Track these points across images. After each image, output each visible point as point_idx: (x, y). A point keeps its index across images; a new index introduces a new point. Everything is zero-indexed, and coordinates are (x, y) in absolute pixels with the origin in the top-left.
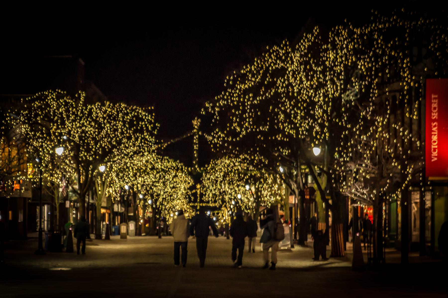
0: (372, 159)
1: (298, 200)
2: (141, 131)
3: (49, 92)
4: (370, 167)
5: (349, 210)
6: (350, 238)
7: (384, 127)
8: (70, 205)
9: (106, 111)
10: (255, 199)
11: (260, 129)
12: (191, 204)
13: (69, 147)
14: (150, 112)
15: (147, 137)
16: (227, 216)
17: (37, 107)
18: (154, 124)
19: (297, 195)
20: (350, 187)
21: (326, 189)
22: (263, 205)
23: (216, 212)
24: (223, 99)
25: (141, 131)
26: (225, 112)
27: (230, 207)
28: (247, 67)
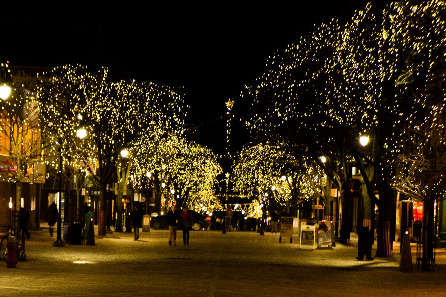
0: (425, 151)
1: (341, 194)
2: (170, 113)
3: (68, 67)
4: (422, 160)
5: (397, 206)
6: (397, 237)
7: (439, 117)
8: (86, 193)
9: (132, 89)
10: (292, 191)
11: (304, 116)
12: (218, 195)
13: (92, 130)
14: (180, 92)
15: (177, 119)
16: (258, 210)
17: (54, 82)
18: (185, 105)
19: (340, 189)
20: (400, 181)
21: (373, 182)
22: (300, 198)
23: (245, 205)
24: (264, 80)
25: (170, 113)
26: (266, 94)
27: (262, 200)
28: (291, 46)
